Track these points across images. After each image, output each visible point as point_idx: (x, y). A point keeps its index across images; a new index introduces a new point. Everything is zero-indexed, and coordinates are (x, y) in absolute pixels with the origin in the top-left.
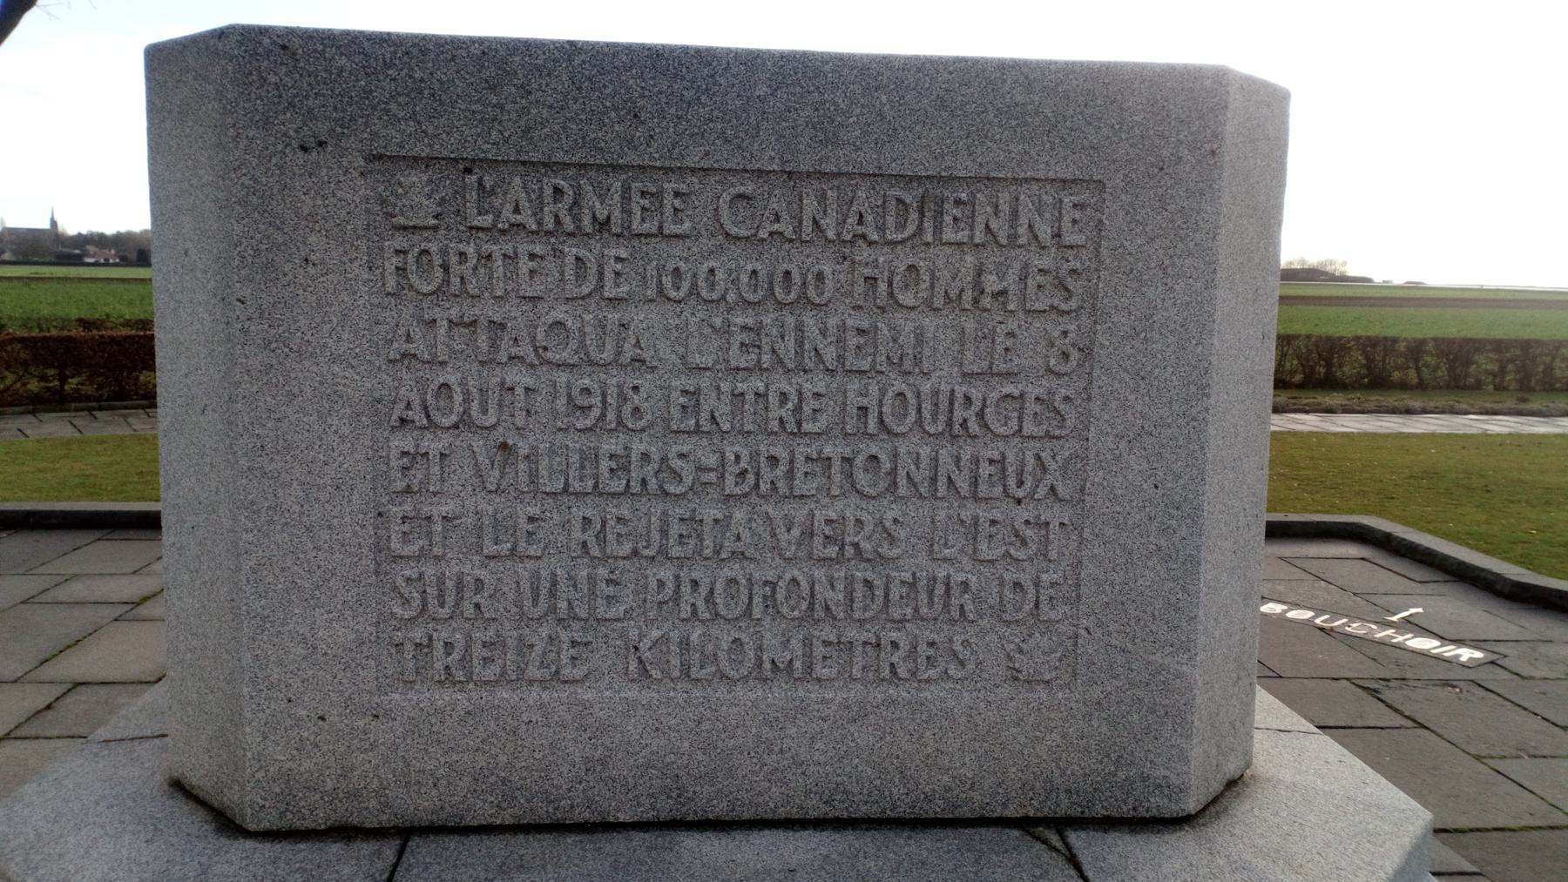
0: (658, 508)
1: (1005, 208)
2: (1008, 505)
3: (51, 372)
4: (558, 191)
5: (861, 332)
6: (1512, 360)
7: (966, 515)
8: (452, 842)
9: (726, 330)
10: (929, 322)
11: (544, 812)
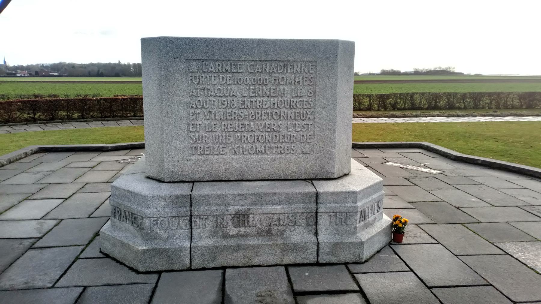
0: (237, 122)
1: (299, 66)
2: (301, 121)
3: (31, 112)
4: (219, 65)
5: (274, 89)
6: (494, 99)
7: (293, 123)
8: (202, 183)
9: (249, 90)
10: (286, 87)
11: (218, 178)
